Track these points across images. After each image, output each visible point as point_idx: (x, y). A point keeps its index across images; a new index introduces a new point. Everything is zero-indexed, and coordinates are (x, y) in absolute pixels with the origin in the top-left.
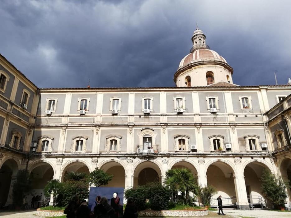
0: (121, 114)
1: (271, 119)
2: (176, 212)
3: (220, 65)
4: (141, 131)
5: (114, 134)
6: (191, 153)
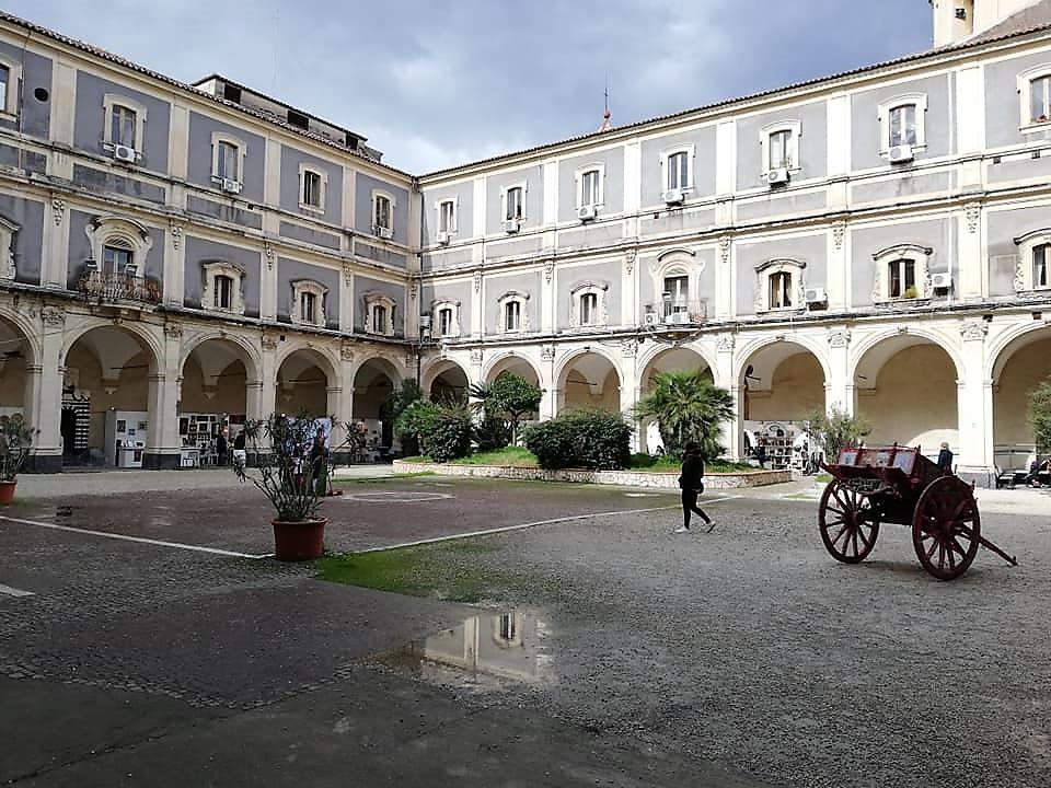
2: (633, 476)
6: (808, 313)
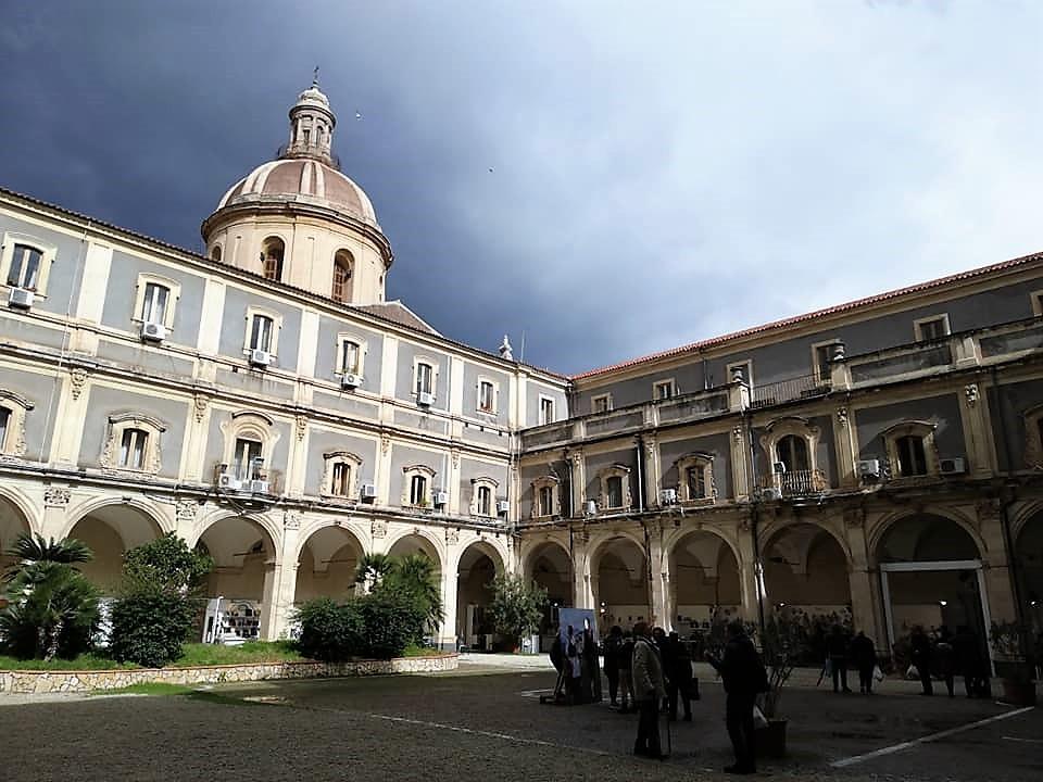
0: (173, 345)
1: (529, 449)
2: (419, 662)
3: (377, 244)
4: (234, 417)
5: (139, 410)
6: (359, 504)
